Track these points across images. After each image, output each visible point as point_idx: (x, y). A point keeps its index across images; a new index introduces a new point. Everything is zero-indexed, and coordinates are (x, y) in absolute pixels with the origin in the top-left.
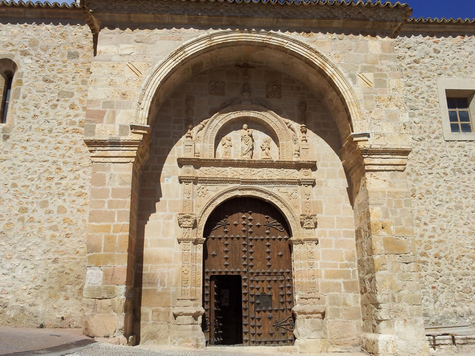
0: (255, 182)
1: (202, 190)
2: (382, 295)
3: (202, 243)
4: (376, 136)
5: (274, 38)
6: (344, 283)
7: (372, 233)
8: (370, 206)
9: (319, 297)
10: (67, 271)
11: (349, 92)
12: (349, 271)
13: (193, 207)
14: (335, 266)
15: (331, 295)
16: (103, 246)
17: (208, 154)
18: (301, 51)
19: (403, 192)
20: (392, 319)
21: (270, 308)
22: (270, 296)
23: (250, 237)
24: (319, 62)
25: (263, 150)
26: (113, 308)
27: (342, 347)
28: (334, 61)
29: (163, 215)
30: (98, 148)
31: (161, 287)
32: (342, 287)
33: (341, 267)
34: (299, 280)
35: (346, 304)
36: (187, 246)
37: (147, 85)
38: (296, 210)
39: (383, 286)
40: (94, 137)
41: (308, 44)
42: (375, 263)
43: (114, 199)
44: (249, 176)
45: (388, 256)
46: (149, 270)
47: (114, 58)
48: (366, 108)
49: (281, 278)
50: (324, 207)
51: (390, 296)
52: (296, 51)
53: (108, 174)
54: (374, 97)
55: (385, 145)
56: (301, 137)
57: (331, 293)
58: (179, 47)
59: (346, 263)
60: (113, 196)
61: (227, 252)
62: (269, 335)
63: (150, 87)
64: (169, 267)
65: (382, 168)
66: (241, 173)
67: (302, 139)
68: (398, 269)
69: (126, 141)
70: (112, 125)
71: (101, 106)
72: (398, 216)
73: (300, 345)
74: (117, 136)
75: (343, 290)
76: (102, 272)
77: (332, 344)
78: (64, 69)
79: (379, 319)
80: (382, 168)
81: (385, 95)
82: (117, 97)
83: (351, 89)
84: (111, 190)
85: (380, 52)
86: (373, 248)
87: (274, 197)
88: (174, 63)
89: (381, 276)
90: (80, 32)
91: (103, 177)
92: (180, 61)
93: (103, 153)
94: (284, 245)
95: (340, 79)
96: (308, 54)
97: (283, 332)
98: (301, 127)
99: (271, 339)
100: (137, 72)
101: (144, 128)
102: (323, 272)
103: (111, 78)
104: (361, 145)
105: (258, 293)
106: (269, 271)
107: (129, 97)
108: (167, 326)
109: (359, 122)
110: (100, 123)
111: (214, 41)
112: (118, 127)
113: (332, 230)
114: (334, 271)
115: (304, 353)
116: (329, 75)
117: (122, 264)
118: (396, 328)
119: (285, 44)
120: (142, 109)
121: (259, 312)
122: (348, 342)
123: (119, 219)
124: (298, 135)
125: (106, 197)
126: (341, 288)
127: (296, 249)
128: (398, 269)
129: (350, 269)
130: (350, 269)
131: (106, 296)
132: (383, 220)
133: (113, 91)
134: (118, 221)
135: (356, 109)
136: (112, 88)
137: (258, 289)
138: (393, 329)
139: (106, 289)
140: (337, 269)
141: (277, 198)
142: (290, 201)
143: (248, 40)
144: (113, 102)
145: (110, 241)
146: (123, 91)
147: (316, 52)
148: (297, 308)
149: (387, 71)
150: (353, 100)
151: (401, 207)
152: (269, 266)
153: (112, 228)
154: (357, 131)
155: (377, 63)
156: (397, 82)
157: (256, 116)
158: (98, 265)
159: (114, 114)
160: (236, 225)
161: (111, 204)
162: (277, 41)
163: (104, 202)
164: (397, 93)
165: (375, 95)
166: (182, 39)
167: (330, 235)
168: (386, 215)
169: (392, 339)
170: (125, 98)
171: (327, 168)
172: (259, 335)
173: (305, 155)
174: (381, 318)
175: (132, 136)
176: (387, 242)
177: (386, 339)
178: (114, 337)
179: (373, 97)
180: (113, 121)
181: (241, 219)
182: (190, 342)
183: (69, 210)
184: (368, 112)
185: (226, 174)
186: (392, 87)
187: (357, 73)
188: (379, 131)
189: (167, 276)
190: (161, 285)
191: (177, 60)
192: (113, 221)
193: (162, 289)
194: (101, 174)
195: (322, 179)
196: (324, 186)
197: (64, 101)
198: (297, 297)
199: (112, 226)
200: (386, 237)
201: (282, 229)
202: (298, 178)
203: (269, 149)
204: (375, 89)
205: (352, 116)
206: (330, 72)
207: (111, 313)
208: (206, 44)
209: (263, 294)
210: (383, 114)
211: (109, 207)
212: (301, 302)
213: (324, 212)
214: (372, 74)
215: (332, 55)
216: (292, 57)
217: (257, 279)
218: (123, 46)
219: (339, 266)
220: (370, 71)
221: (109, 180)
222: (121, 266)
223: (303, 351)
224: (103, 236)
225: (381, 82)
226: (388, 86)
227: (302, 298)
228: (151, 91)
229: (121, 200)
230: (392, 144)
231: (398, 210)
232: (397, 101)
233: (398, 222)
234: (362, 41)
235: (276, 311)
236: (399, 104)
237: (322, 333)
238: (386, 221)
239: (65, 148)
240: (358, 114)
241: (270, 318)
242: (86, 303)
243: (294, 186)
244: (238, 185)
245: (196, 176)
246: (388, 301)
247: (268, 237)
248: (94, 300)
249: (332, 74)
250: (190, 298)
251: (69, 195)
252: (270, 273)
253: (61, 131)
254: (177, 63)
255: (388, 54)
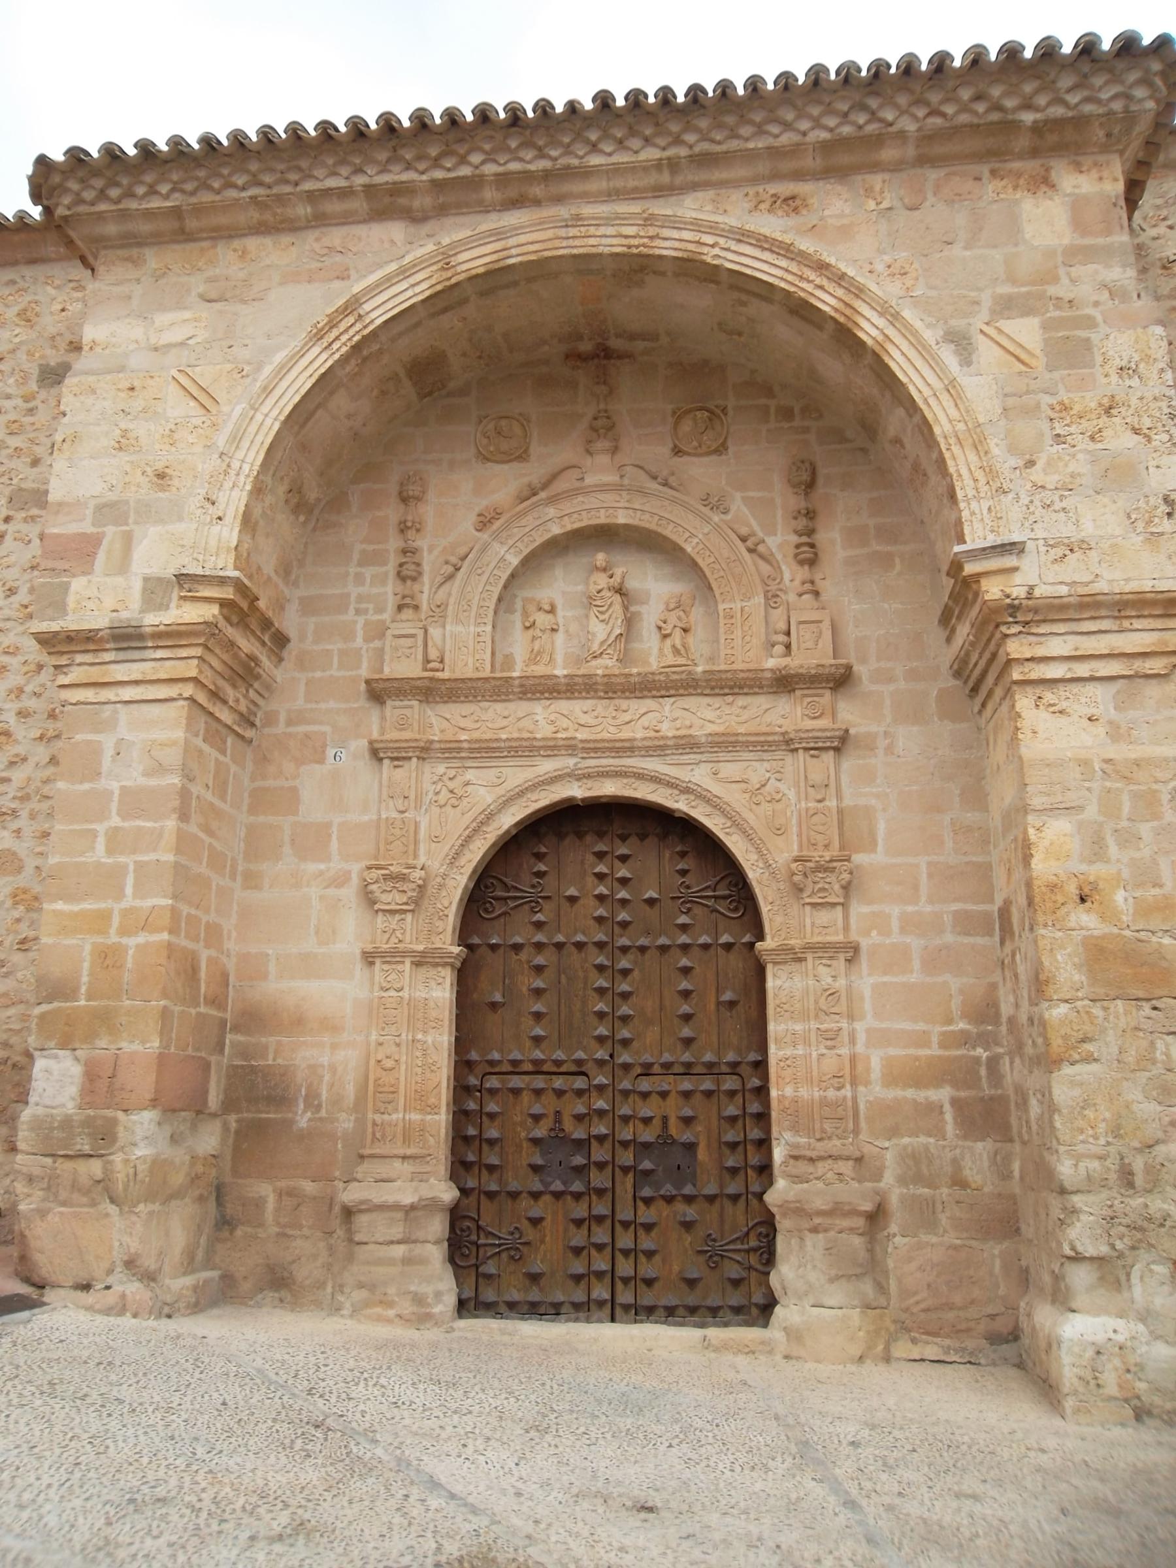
0: (627, 748)
1: (451, 785)
2: (1078, 1158)
3: (445, 965)
4: (1052, 551)
5: (666, 233)
6: (954, 1102)
7: (1041, 918)
8: (1030, 818)
9: (857, 1154)
10: (18, 1058)
11: (944, 397)
12: (977, 1060)
13: (416, 842)
14: (922, 1040)
15: (905, 1148)
16: (85, 979)
17: (470, 661)
18: (765, 267)
19: (1166, 759)
20: (1121, 1255)
21: (688, 1190)
22: (691, 1147)
23: (624, 941)
24: (832, 301)
25: (665, 636)
26: (107, 1189)
27: (947, 1342)
28: (888, 290)
29: (321, 873)
30: (79, 658)
31: (309, 1114)
32: (949, 1117)
33: (942, 1045)
34: (789, 1091)
35: (963, 1184)
36: (393, 976)
37: (236, 439)
38: (780, 841)
39: (1080, 1123)
40: (62, 623)
41: (787, 238)
42: (1051, 1034)
43: (126, 824)
44: (611, 729)
45: (1105, 1009)
46: (271, 1057)
47: (134, 362)
48: (1012, 450)
49: (730, 1083)
50: (881, 828)
51: (1112, 1164)
52: (748, 271)
53: (108, 742)
54: (1044, 407)
55: (1087, 584)
56: (797, 582)
57: (906, 1140)
58: (341, 302)
59: (962, 1031)
60: (124, 816)
61: (538, 992)
62: (683, 1286)
63: (245, 444)
64: (334, 1047)
65: (1082, 670)
66: (584, 719)
67: (801, 589)
68: (1147, 1059)
69: (162, 628)
70: (119, 580)
71: (89, 519)
72: (1146, 852)
73: (785, 1329)
74: (136, 615)
75: (950, 1128)
76: (77, 1070)
77: (908, 1330)
78: (28, 420)
79: (1068, 1252)
80: (1082, 670)
81: (1088, 395)
82: (139, 486)
83: (952, 387)
84: (117, 793)
85: (1068, 238)
86: (1042, 977)
87: (700, 797)
88: (324, 356)
89: (1073, 1083)
90: (78, 300)
91: (95, 751)
92: (344, 349)
93: (95, 674)
94: (735, 963)
95: (912, 354)
96: (790, 278)
97: (734, 1276)
98: (798, 546)
99: (691, 1300)
100: (204, 399)
101: (222, 581)
102: (876, 1063)
103: (123, 426)
104: (992, 590)
105: (648, 1135)
106: (687, 1057)
107: (176, 482)
108: (322, 1245)
109: (985, 505)
110: (84, 573)
111: (459, 269)
112: (138, 585)
113: (910, 909)
114: (917, 1058)
115: (798, 1358)
116: (869, 342)
117: (143, 1042)
118: (1138, 1291)
119: (705, 250)
120: (220, 518)
121: (648, 1201)
122: (972, 1324)
123: (139, 892)
124: (787, 576)
125: (102, 815)
126: (943, 1121)
127: (779, 982)
128: (1147, 1059)
129: (979, 1051)
130: (979, 1050)
131: (87, 1149)
132: (1084, 867)
133: (128, 468)
134: (135, 896)
135: (972, 457)
136: (124, 457)
137: (647, 1121)
138: (1126, 1294)
139: (88, 1122)
140: (928, 1052)
141: (708, 801)
142: (750, 804)
143: (575, 251)
144: (127, 502)
145: (108, 962)
146: (159, 466)
147: (822, 267)
148: (780, 1192)
149: (1096, 304)
150: (961, 426)
151: (1156, 816)
152: (688, 1042)
153: (116, 921)
154: (977, 536)
155: (1056, 280)
156: (1136, 342)
157: (636, 522)
158: (66, 1043)
159: (128, 540)
160: (572, 900)
161: (115, 840)
162: (677, 244)
163: (94, 834)
164: (1135, 382)
165: (1047, 399)
166: (352, 272)
167: (903, 930)
168: (1096, 849)
169: (1120, 1338)
170: (162, 489)
171: (892, 687)
172: (649, 1282)
173: (810, 644)
174: (1073, 1248)
175: (179, 612)
176: (1097, 953)
177: (1091, 1338)
178: (108, 1288)
179: (1038, 406)
180: (123, 566)
181: (590, 880)
182: (390, 1304)
183: (30, 863)
184: (1021, 463)
185: (532, 727)
186: (1118, 363)
187: (978, 322)
188: (1067, 531)
189: (326, 1078)
190: (308, 1106)
191: (335, 346)
192: (120, 895)
193: (310, 1120)
194: (89, 742)
195: (874, 728)
196: (880, 752)
197: (25, 520)
198: (779, 1154)
199: (116, 912)
200: (1096, 933)
201: (736, 910)
202: (782, 730)
203: (685, 630)
204: (1048, 376)
205: (958, 485)
206: (874, 332)
207: (101, 1207)
208: (433, 281)
209: (666, 1141)
210: (1080, 465)
211: (110, 851)
212: (794, 1171)
213: (880, 848)
214: (1034, 322)
215: (879, 267)
216: (744, 297)
217: (645, 1085)
218: (162, 319)
219: (935, 1040)
220: (1027, 312)
221: (113, 761)
222: (140, 1048)
223: (795, 1354)
224: (88, 948)
225: (1070, 349)
226: (1099, 359)
227: (796, 1158)
228: (249, 459)
229: (149, 824)
230: (1117, 575)
231: (1145, 829)
232: (1137, 413)
233: (1146, 876)
234: (995, 207)
235: (711, 1199)
236: (1147, 422)
237: (867, 1287)
238: (1096, 871)
239: (25, 669)
240: (979, 474)
241: (688, 1226)
242: (25, 1170)
243: (766, 756)
244: (571, 762)
245: (425, 737)
246: (1104, 1184)
247: (684, 939)
248: (49, 1160)
249: (880, 338)
250: (401, 1152)
251: (33, 816)
252: (689, 1065)
253: (14, 614)
254: (337, 356)
255: (1100, 241)
